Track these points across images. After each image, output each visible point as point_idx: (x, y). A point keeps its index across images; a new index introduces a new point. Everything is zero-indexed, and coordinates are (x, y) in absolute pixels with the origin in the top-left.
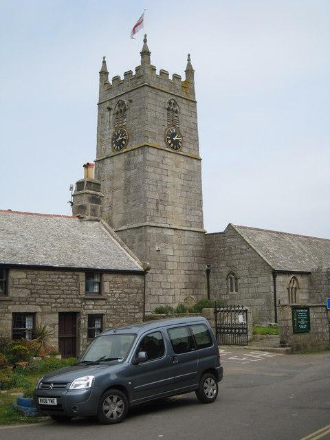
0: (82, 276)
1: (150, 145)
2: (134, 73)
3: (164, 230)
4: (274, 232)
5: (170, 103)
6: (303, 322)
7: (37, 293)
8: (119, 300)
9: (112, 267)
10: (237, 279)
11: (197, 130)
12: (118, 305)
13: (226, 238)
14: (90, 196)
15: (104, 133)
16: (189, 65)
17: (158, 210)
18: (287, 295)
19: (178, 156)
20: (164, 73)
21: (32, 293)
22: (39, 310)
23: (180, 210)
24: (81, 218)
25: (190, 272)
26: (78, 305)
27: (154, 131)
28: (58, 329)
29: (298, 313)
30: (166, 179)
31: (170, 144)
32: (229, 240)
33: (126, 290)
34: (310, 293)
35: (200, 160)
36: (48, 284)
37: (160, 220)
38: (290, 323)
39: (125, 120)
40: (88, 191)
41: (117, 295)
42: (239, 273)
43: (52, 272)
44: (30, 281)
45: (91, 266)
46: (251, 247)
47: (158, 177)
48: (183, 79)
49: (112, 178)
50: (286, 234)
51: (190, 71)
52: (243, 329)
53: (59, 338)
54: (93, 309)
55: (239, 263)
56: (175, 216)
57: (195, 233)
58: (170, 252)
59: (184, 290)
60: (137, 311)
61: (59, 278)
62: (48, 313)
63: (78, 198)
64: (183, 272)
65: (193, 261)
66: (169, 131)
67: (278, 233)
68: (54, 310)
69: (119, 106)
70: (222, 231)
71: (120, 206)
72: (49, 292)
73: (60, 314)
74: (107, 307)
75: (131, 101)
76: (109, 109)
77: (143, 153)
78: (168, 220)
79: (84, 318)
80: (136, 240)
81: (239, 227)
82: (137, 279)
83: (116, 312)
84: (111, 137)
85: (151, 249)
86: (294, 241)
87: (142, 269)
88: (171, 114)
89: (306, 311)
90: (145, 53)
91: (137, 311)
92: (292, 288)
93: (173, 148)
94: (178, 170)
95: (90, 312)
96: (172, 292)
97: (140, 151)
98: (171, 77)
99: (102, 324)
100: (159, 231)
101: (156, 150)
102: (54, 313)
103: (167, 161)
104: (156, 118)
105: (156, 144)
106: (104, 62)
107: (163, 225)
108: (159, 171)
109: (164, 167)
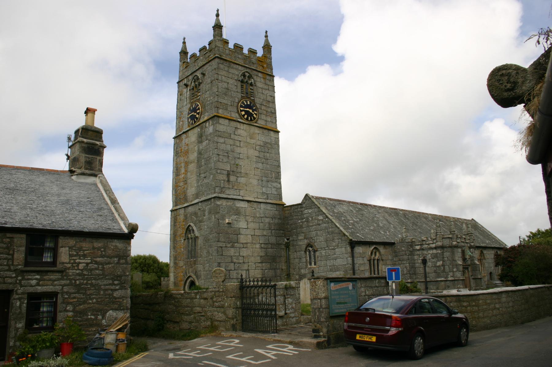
0: (21, 240)
1: (220, 115)
3: (236, 202)
4: (358, 203)
5: (244, 75)
8: (85, 273)
9: (75, 226)
10: (315, 251)
11: (274, 102)
13: (303, 209)
17: (228, 181)
18: (367, 267)
19: (253, 127)
20: (238, 48)
23: (255, 182)
25: (266, 246)
26: (10, 281)
27: (224, 101)
30: (238, 150)
31: (244, 116)
32: (306, 211)
33: (98, 259)
35: (278, 132)
37: (231, 192)
39: (199, 94)
41: (81, 266)
42: (317, 245)
46: (327, 217)
47: (229, 148)
48: (260, 53)
51: (267, 47)
52: (271, 310)
54: (38, 284)
55: (317, 235)
56: (250, 187)
57: (275, 206)
59: (260, 265)
64: (258, 246)
65: (270, 234)
66: (243, 103)
67: (361, 204)
69: (195, 82)
70: (300, 201)
74: (63, 282)
75: (204, 74)
76: (186, 85)
77: (213, 124)
78: (241, 192)
79: (20, 299)
80: (207, 213)
81: (317, 198)
83: (79, 288)
85: (221, 221)
87: (126, 231)
88: (245, 87)
90: (218, 27)
91: (117, 288)
93: (247, 119)
94: (253, 141)
95: (31, 290)
96: (245, 267)
97: (211, 122)
98: (245, 51)
100: (230, 203)
103: (239, 132)
105: (228, 115)
106: (184, 43)
107: (235, 197)
108: (231, 142)
109: (236, 138)
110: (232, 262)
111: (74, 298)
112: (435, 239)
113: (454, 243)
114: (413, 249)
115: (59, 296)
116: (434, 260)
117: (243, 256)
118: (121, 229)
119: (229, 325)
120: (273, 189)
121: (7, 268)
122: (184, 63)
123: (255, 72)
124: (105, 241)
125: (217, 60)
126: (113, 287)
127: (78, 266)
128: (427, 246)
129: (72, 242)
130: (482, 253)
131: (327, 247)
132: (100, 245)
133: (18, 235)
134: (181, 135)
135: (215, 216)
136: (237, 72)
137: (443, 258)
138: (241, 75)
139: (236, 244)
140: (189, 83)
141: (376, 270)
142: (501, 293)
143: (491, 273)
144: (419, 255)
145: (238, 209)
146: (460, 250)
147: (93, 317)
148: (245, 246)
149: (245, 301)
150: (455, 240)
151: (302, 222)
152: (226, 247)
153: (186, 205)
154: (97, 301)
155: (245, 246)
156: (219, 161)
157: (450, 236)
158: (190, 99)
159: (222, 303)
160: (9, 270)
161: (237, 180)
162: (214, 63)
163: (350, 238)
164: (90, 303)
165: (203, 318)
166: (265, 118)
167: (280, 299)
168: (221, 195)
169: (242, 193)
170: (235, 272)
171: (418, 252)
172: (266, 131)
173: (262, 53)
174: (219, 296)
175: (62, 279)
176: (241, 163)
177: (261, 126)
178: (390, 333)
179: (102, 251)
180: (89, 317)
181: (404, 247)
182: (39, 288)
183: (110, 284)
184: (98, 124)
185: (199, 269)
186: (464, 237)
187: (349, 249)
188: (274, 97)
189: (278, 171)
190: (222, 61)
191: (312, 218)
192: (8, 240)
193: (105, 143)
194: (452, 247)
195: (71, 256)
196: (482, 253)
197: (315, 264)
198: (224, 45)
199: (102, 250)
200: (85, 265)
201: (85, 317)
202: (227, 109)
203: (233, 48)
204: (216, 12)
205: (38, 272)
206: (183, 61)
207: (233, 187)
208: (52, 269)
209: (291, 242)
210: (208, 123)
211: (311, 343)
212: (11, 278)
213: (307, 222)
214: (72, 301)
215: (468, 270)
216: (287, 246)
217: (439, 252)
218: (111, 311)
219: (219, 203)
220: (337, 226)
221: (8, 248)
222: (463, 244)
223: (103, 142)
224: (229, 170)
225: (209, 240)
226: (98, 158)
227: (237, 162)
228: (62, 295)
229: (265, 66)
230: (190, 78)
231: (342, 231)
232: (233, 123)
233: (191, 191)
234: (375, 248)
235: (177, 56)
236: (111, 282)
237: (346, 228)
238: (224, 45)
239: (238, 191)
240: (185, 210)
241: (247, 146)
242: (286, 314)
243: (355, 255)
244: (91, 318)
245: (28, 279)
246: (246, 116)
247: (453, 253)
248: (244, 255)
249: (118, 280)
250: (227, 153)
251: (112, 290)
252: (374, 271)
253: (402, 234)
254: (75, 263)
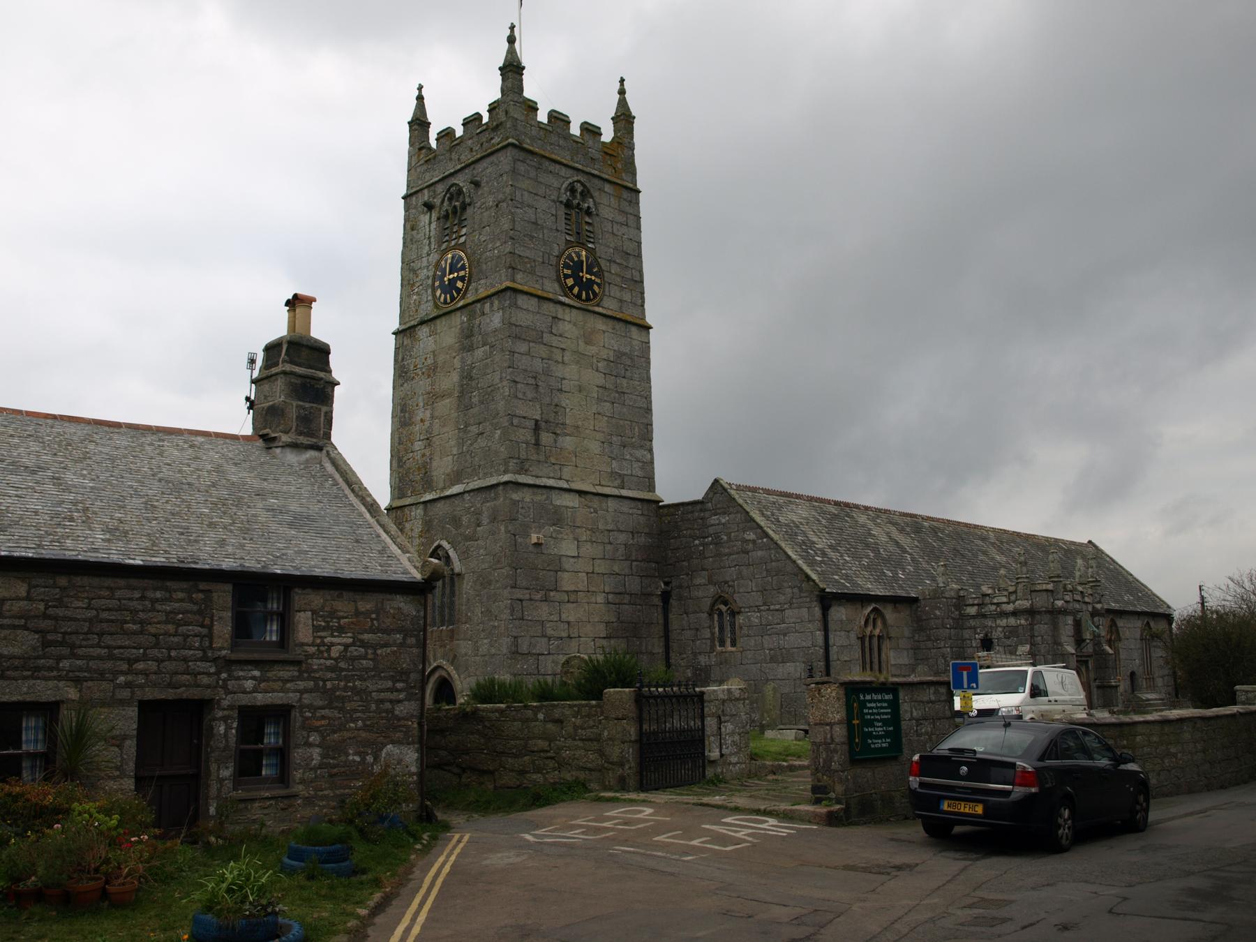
0: (223, 596)
1: (520, 287)
2: (485, 119)
3: (554, 495)
4: (829, 502)
5: (572, 190)
6: (879, 729)
7: (62, 644)
8: (342, 665)
9: (324, 570)
10: (733, 614)
11: (639, 256)
12: (339, 679)
13: (707, 514)
14: (298, 381)
15: (416, 265)
16: (623, 103)
17: (537, 444)
18: (857, 654)
20: (558, 119)
21: (46, 644)
22: (73, 694)
23: (595, 447)
24: (268, 441)
26: (205, 680)
27: (528, 253)
28: (134, 750)
29: (863, 704)
30: (559, 371)
32: (714, 519)
33: (366, 637)
34: (916, 649)
36: (105, 615)
38: (840, 732)
39: (464, 231)
40: (288, 367)
41: (335, 651)
42: (740, 600)
43: (122, 582)
44: (42, 606)
45: (252, 564)
46: (767, 535)
47: (538, 365)
48: (607, 135)
49: (432, 370)
50: (857, 506)
51: (624, 118)
53: (140, 781)
54: (255, 690)
56: (584, 461)
57: (633, 504)
58: (567, 548)
59: (605, 643)
60: (402, 696)
61: (143, 598)
62: (104, 704)
63: (266, 387)
64: (600, 598)
65: (627, 571)
67: (837, 503)
68: (126, 694)
69: (450, 199)
70: (699, 496)
71: (447, 436)
72: (108, 640)
73: (146, 707)
74: (301, 685)
75: (477, 184)
76: (429, 207)
78: (565, 469)
79: (225, 719)
80: (485, 521)
81: (739, 488)
82: (404, 605)
84: (431, 274)
86: (877, 525)
87: (417, 576)
89: (889, 697)
90: (512, 70)
91: (402, 696)
92: (871, 637)
93: (579, 297)
94: (592, 350)
95: (244, 700)
97: (496, 302)
98: (575, 130)
99: (287, 735)
100: (540, 497)
101: (534, 301)
102: (122, 703)
103: (565, 327)
104: (535, 223)
106: (420, 98)
107: (551, 482)
108: (542, 351)
109: (555, 341)
110: (544, 636)
111: (323, 717)
112: (1015, 592)
113: (1059, 603)
114: (961, 614)
115: (295, 714)
116: (1008, 642)
117: (568, 623)
118: (406, 572)
119: (611, 777)
120: (635, 465)
121: (199, 654)
122: (420, 149)
123: (596, 181)
124: (380, 596)
125: (510, 152)
126: (394, 696)
127: (329, 651)
128: (993, 607)
129: (317, 599)
130: (1113, 627)
131: (765, 604)
132: (368, 607)
133: (220, 586)
134: (414, 326)
135: (506, 527)
136: (559, 182)
137: (1032, 636)
138: (566, 189)
139: (552, 594)
140: (437, 201)
141: (876, 660)
142: (1181, 720)
143: (1133, 674)
144: (975, 628)
145: (557, 509)
146: (1070, 620)
147: (357, 759)
148: (573, 598)
149: (645, 727)
150: (1060, 596)
151: (702, 544)
152: (531, 600)
153: (428, 497)
154: (365, 725)
155: (573, 598)
156: (516, 397)
157: (1050, 587)
158: (440, 243)
159: (595, 730)
160: (204, 659)
161: (556, 441)
162: (505, 159)
163: (822, 585)
164: (350, 729)
165: (551, 764)
166: (618, 295)
167: (711, 723)
168: (522, 479)
169: (566, 472)
170: (551, 657)
171: (972, 622)
172: (621, 324)
173: (612, 135)
174: (588, 716)
175: (300, 678)
176: (565, 401)
177: (610, 313)
178: (1013, 797)
179: (372, 620)
180: (351, 758)
181: (939, 608)
182: (259, 696)
183: (388, 690)
184: (318, 331)
185: (463, 651)
186: (1080, 588)
187: (817, 611)
188: (639, 243)
189: (645, 421)
190: (522, 155)
191: (729, 535)
192: (201, 596)
193: (336, 375)
194: (1055, 613)
195: (316, 629)
196: (1113, 624)
197: (880, 671)
198: (527, 115)
199: (374, 616)
200: (342, 648)
201: (343, 758)
202: (532, 273)
203: (545, 121)
204: (508, 32)
205: (256, 663)
206: (417, 146)
207: (547, 457)
208: (282, 656)
209: (674, 593)
210: (487, 305)
211: (816, 815)
212: (209, 674)
213: (716, 544)
214: (318, 723)
215: (1087, 668)
216: (666, 597)
217: (1023, 622)
218: (389, 746)
219: (515, 496)
220: (789, 557)
221: (200, 612)
222: (1077, 606)
223: (330, 372)
224: (538, 417)
225: (490, 583)
226: (324, 409)
227: (556, 400)
228: (301, 712)
229: (619, 166)
230: (440, 188)
231: (801, 570)
232: (549, 308)
233: (442, 466)
234: (875, 609)
235: (403, 134)
236: (390, 684)
237: (812, 563)
238: (527, 115)
239: (557, 467)
240: (425, 510)
241: (578, 362)
242: (722, 755)
243: (831, 626)
244: (354, 761)
245: (238, 678)
246: (576, 290)
247: (1055, 627)
248: (571, 619)
249: (403, 681)
250: (535, 378)
251: (391, 701)
252: (871, 662)
253: (934, 579)
254: (324, 644)
